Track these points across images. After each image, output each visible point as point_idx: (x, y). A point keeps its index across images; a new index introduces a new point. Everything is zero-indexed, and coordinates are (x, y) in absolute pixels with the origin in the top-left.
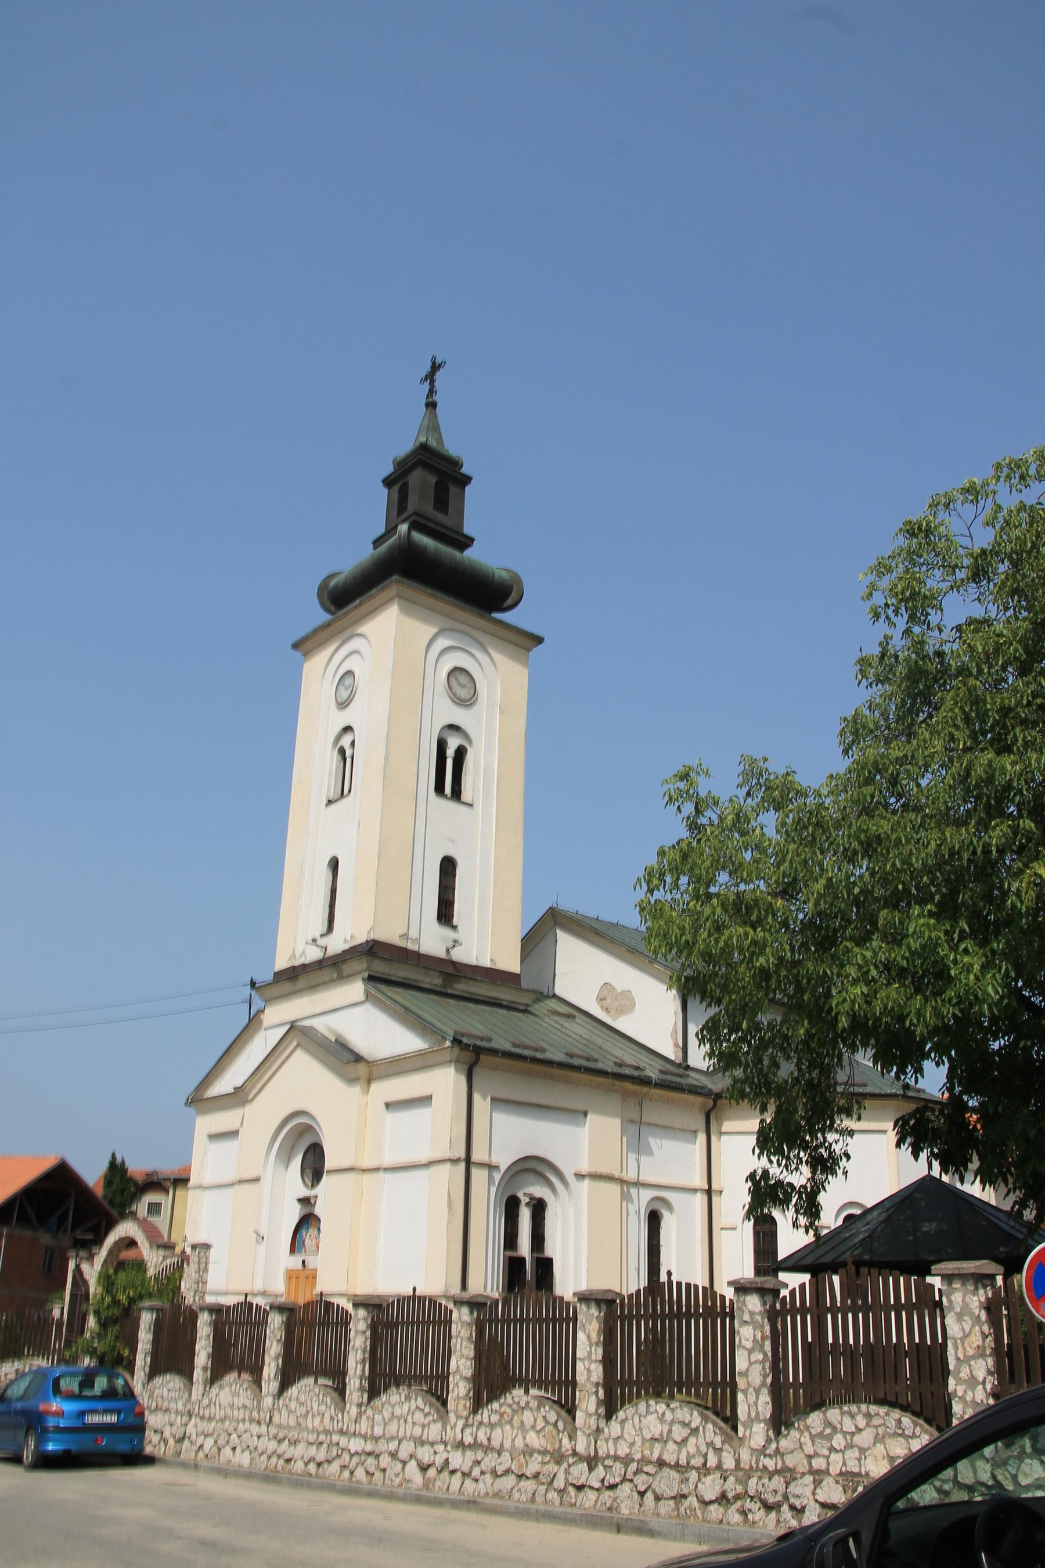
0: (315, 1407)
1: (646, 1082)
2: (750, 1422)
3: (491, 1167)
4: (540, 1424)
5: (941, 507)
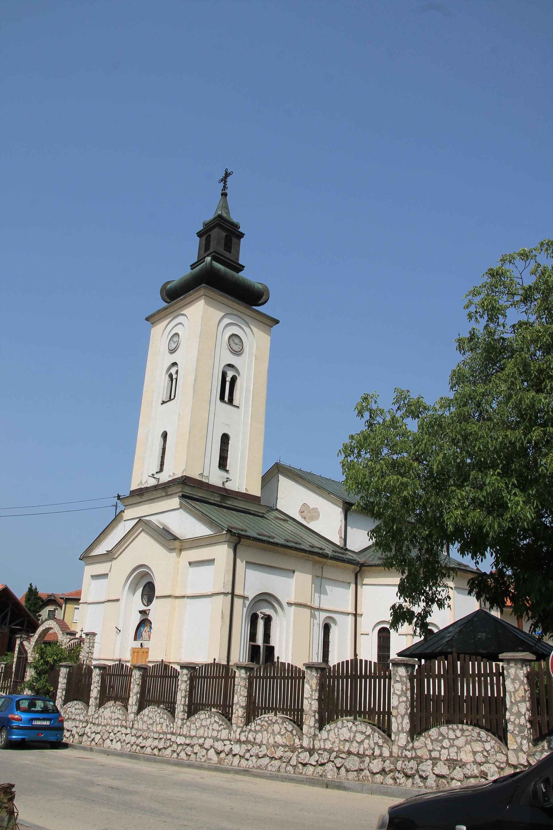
0: (158, 720)
1: (325, 556)
2: (398, 732)
3: (245, 598)
4: (283, 731)
5: (507, 262)
